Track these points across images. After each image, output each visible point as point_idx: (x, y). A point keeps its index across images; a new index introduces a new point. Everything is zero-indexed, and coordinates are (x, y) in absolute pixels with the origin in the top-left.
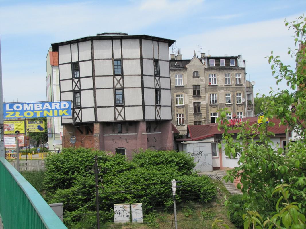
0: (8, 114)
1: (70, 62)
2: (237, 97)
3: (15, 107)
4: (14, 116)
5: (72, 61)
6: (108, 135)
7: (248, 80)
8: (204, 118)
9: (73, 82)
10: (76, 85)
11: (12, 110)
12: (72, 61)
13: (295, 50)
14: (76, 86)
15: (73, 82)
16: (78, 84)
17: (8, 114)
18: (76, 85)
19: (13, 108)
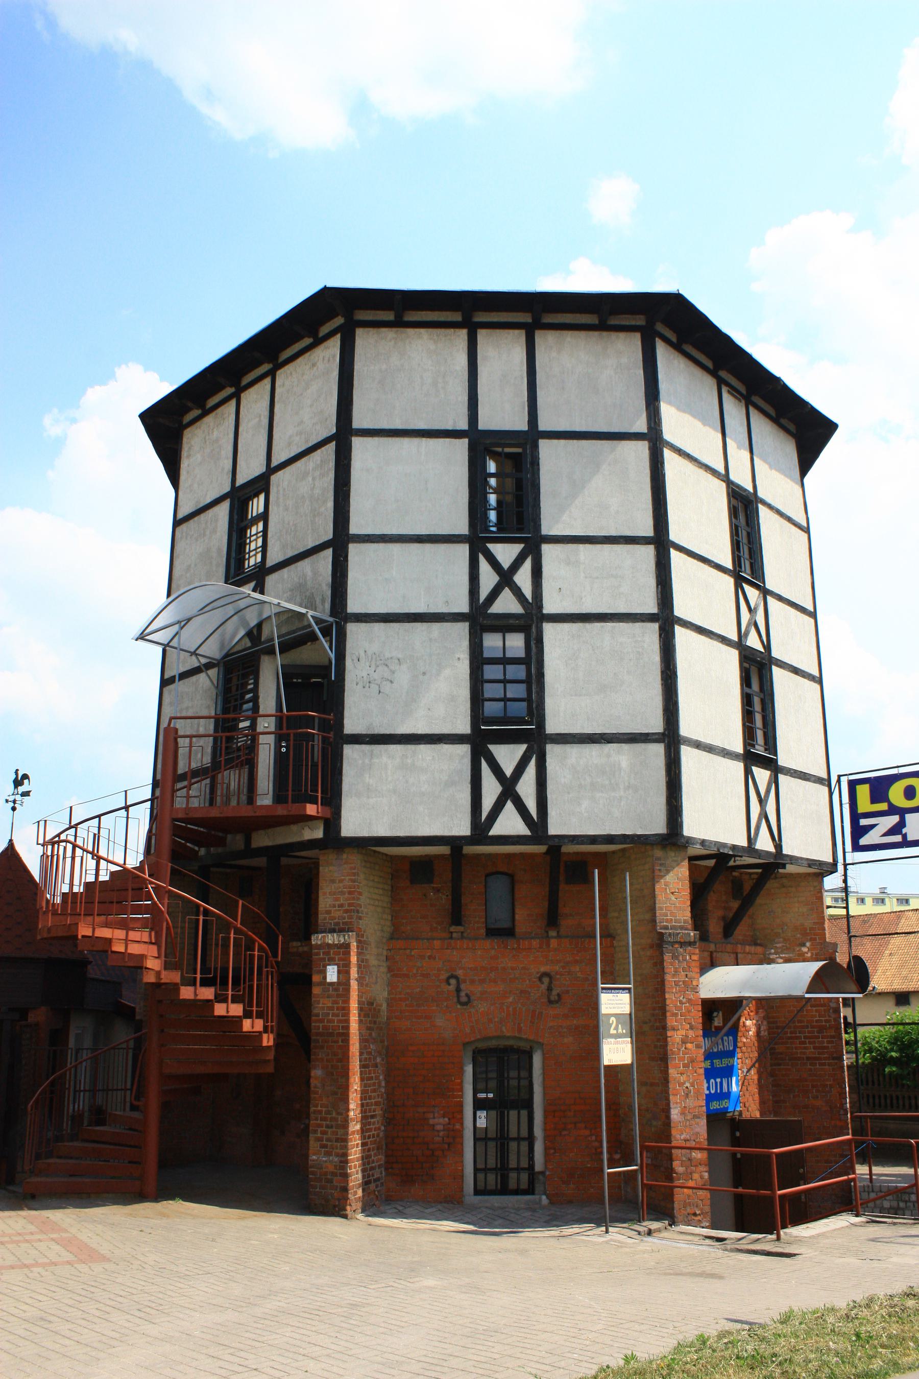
0: (872, 827)
1: (543, 426)
2: (711, 1007)
3: (896, 793)
4: (900, 833)
5: (543, 444)
6: (354, 1106)
7: (149, 789)
8: (828, 1042)
9: (484, 765)
10: (509, 792)
11: (883, 806)
12: (543, 444)
13: (795, 1255)
14: (509, 805)
15: (484, 765)
16: (491, 789)
17: (872, 827)
18: (509, 792)
19: (887, 800)
